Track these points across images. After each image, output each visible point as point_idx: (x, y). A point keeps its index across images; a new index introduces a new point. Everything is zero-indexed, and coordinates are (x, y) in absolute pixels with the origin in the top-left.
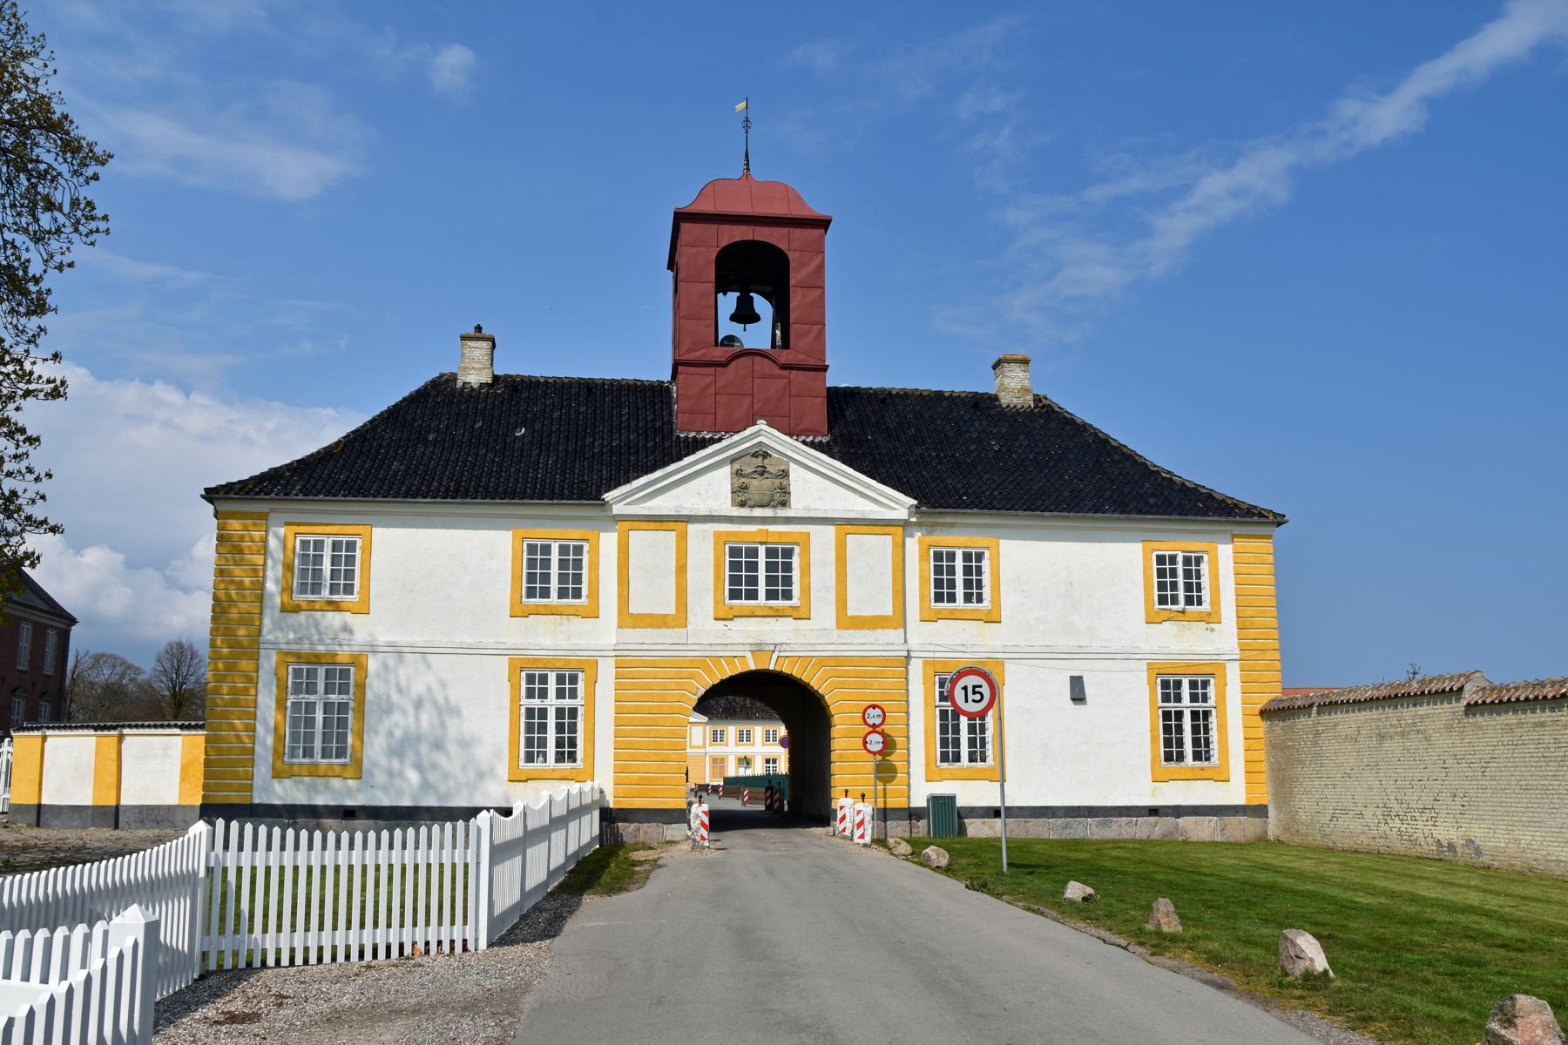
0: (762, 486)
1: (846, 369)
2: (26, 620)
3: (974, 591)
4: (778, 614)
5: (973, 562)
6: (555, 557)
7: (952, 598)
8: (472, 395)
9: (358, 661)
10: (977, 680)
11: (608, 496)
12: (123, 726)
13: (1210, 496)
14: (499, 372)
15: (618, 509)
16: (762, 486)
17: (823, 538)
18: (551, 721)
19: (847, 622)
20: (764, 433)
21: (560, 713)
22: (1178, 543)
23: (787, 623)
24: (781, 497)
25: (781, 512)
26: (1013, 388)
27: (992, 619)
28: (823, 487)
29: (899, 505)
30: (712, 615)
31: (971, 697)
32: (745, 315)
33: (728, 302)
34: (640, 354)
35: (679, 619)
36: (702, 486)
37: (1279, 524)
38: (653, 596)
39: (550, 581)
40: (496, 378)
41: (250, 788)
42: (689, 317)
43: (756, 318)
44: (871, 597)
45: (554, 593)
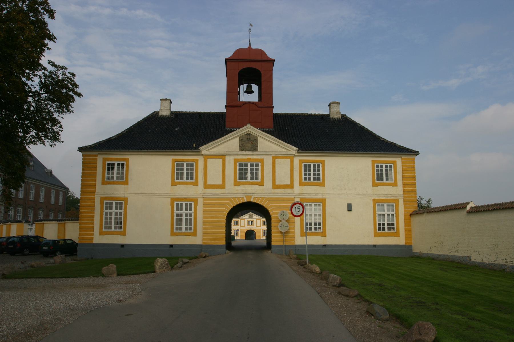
0: (249, 144)
1: (280, 107)
2: (43, 186)
3: (317, 177)
4: (253, 184)
5: (317, 168)
6: (312, 168)
7: (310, 179)
8: (164, 118)
9: (126, 200)
10: (299, 205)
11: (201, 148)
12: (66, 220)
13: (395, 145)
14: (172, 110)
15: (204, 152)
16: (249, 144)
17: (268, 161)
18: (184, 218)
19: (275, 187)
20: (249, 129)
21: (186, 215)
22: (384, 159)
23: (256, 187)
24: (254, 148)
25: (255, 152)
26: (336, 113)
27: (323, 185)
28: (268, 143)
29: (293, 150)
30: (233, 184)
31: (297, 210)
32: (249, 91)
33: (244, 87)
34: (217, 105)
35: (222, 186)
36: (230, 143)
37: (417, 155)
38: (243, 224)
39: (183, 175)
40: (172, 113)
41: (92, 238)
42: (232, 94)
43: (252, 92)
44: (283, 178)
45: (185, 179)
